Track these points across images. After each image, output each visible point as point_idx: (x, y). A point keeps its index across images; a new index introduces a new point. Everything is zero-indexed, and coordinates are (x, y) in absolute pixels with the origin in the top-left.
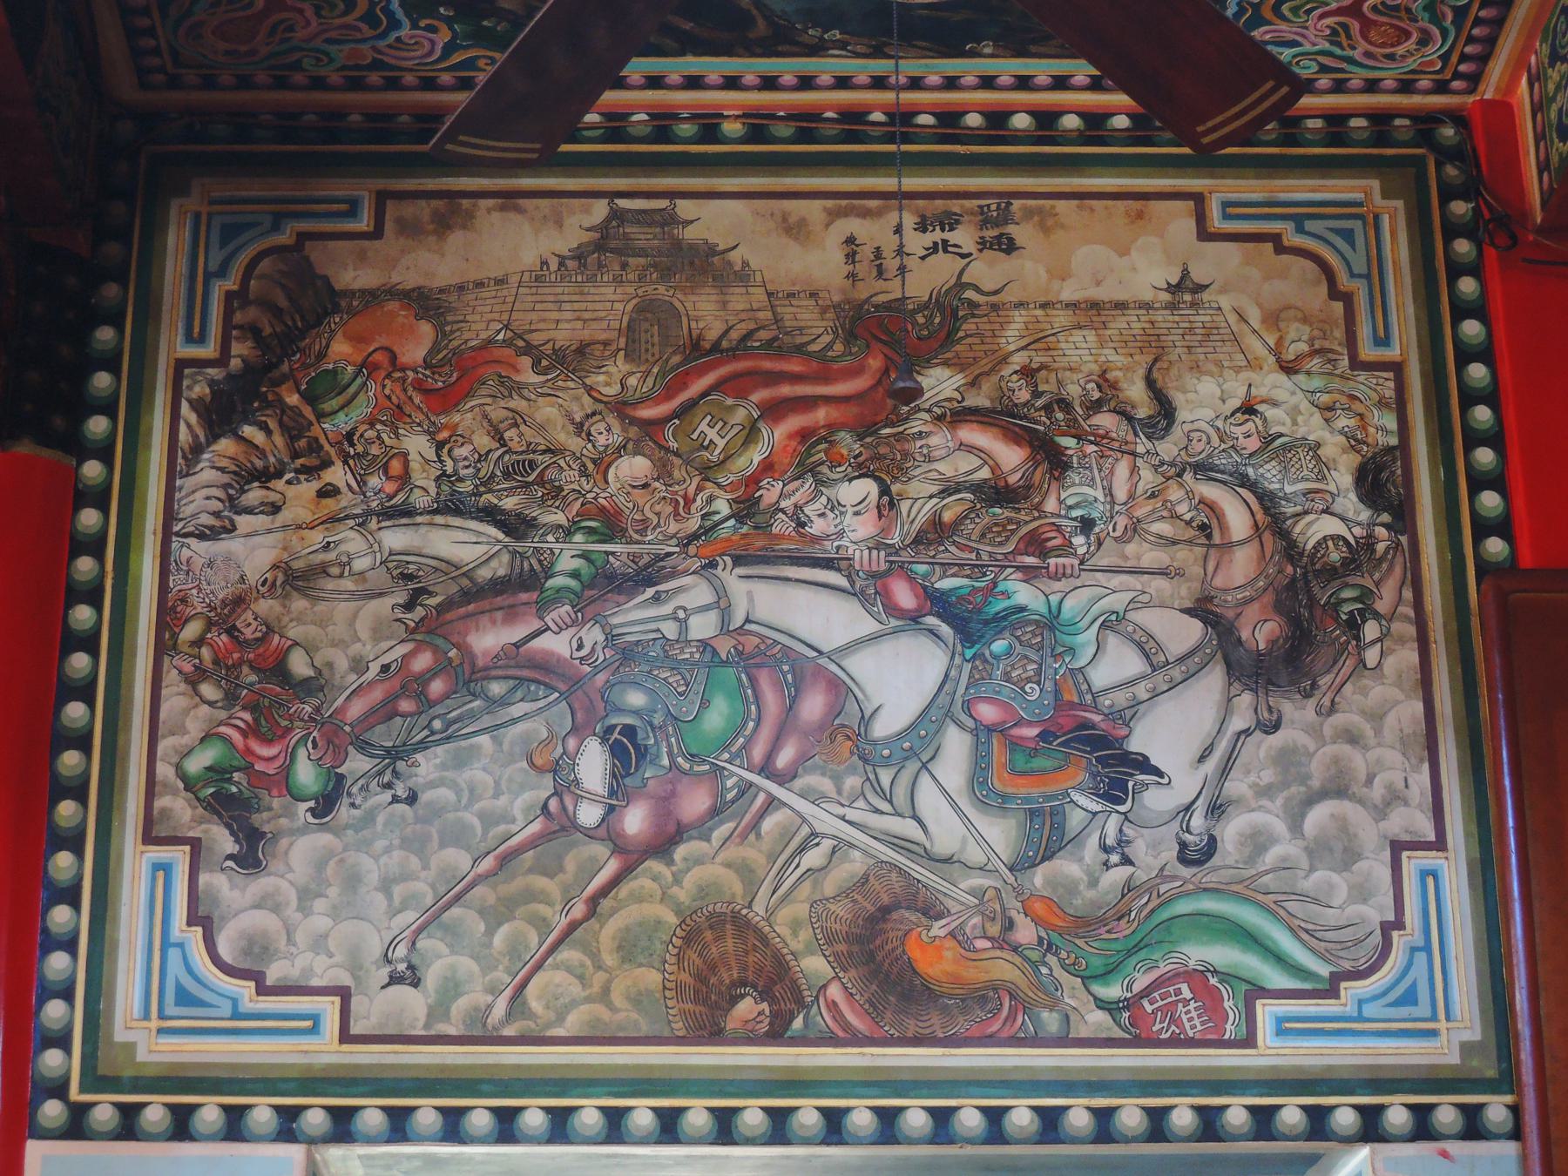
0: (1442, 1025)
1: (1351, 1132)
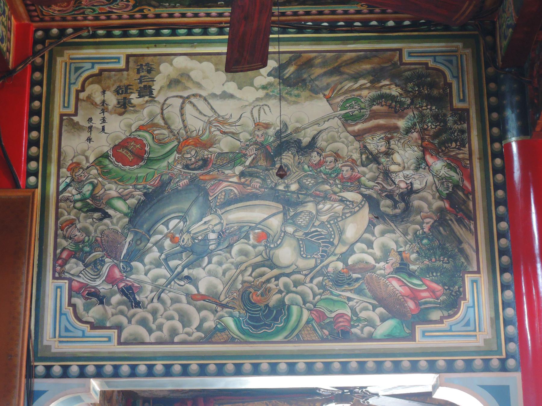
0: (57, 339)
1: (161, 372)
